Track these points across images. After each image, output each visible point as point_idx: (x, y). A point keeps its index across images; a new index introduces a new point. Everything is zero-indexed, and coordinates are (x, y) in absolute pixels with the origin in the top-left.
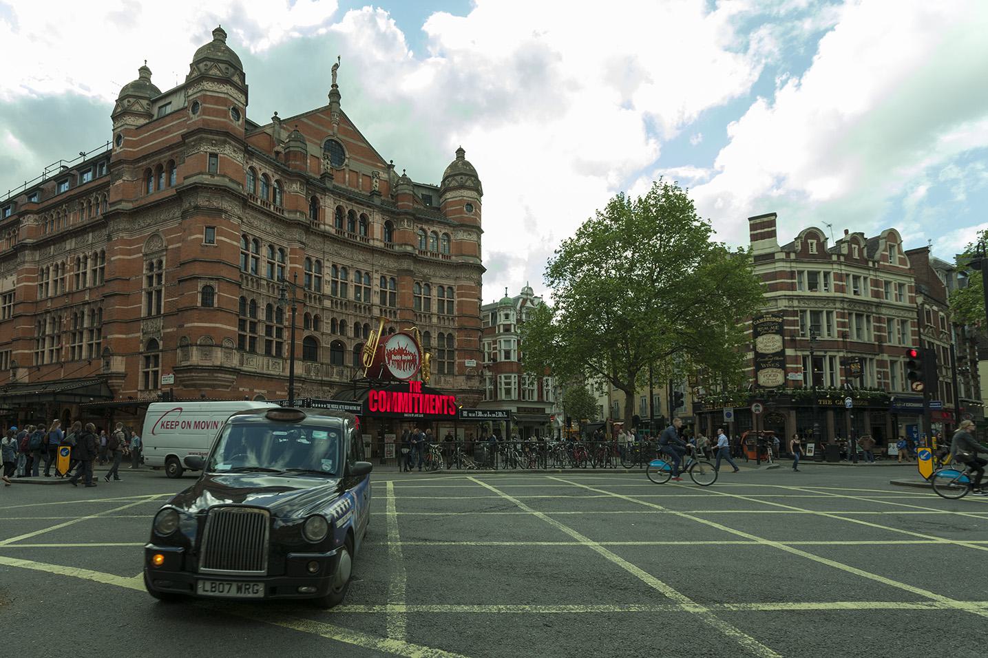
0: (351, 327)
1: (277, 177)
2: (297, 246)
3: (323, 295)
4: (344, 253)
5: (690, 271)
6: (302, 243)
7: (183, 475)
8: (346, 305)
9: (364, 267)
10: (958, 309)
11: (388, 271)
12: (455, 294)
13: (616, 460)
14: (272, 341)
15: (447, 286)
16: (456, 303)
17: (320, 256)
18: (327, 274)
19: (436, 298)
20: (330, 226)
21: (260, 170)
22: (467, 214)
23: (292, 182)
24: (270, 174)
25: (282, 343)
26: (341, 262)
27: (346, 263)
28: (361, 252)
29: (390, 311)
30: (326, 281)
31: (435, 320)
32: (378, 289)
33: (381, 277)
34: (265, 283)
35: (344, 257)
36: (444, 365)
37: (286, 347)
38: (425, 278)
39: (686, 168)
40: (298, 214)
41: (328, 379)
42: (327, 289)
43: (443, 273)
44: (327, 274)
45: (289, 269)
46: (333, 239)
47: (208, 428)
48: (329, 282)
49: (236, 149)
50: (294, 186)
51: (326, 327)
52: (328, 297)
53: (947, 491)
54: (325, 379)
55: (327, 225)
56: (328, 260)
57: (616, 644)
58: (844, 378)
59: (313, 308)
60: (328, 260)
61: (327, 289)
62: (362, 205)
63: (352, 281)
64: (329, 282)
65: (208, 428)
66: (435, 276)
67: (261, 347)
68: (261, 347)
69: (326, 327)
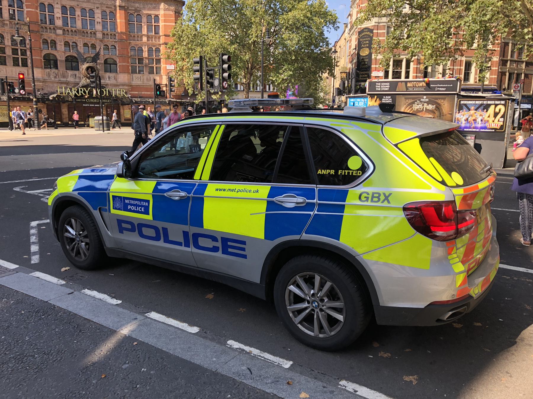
3: (56, 27)
5: (34, 224)
10: (528, 22)
11: (107, 7)
14: (18, 58)
25: (27, 59)
30: (57, 17)
31: (145, 39)
32: (100, 20)
33: (102, 12)
34: (8, 22)
36: (153, 61)
37: (29, 61)
39: (72, 207)
41: (65, 79)
45: (26, 12)
48: (60, 18)
51: (60, 46)
53: (431, 134)
54: (62, 79)
56: (57, 3)
58: (415, 75)
59: (49, 36)
60: (57, 3)
63: (78, 16)
64: (60, 18)
66: (144, 9)
69: (60, 46)
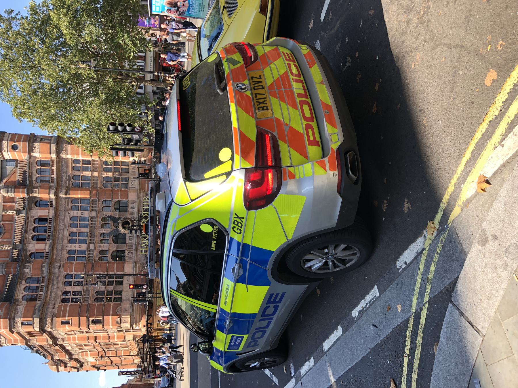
0: (104, 230)
1: (24, 282)
2: (62, 269)
4: (61, 235)
6: (60, 266)
7: (304, 106)
8: (92, 233)
9: (67, 222)
12: (70, 273)
13: (211, 29)
15: (69, 237)
16: (76, 273)
17: (65, 252)
18: (75, 247)
19: (78, 228)
20: (46, 246)
21: (22, 293)
22: (20, 149)
23: (24, 273)
24: (23, 287)
26: (66, 238)
27: (66, 234)
28: (58, 223)
29: (92, 204)
30: (79, 248)
31: (95, 174)
35: (63, 235)
38: (69, 180)
40: (43, 269)
42: (84, 247)
43: (62, 224)
44: (75, 247)
46: (53, 244)
47: (261, 82)
48: (79, 246)
49: (16, 313)
50: (26, 271)
51: (105, 247)
52: (89, 246)
55: (45, 247)
57: (391, 16)
61: (84, 247)
62: (28, 223)
65: (261, 82)
66: (67, 172)
67: (119, 288)
68: (119, 288)
